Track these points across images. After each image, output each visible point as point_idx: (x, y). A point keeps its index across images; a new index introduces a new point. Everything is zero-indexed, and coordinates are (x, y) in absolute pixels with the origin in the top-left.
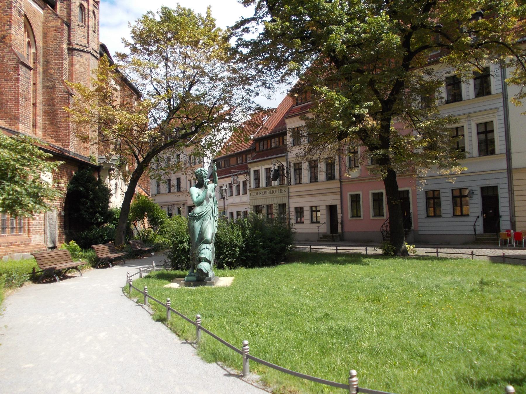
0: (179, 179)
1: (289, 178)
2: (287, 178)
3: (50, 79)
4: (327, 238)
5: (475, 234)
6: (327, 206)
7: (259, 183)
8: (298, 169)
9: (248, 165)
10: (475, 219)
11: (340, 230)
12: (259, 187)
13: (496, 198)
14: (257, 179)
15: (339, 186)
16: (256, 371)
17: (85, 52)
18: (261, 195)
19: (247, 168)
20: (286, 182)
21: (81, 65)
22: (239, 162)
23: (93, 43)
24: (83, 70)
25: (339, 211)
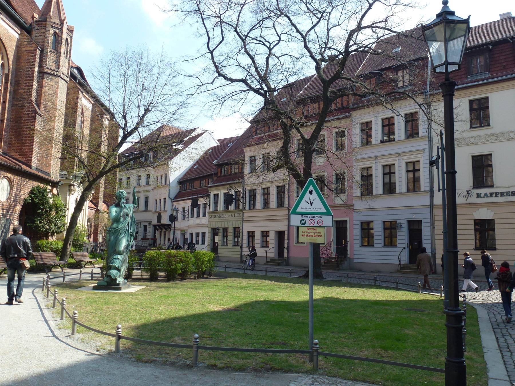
0: (147, 198)
1: (244, 204)
2: (243, 203)
3: (20, 99)
4: (273, 262)
5: (400, 264)
6: (276, 232)
7: (217, 207)
8: (253, 195)
9: (209, 189)
10: (400, 250)
11: (286, 255)
12: (217, 210)
13: (420, 231)
14: (216, 203)
17: (55, 75)
18: (218, 218)
19: (208, 192)
20: (241, 208)
21: (50, 88)
22: (202, 185)
23: (63, 68)
24: (51, 92)
25: (286, 237)
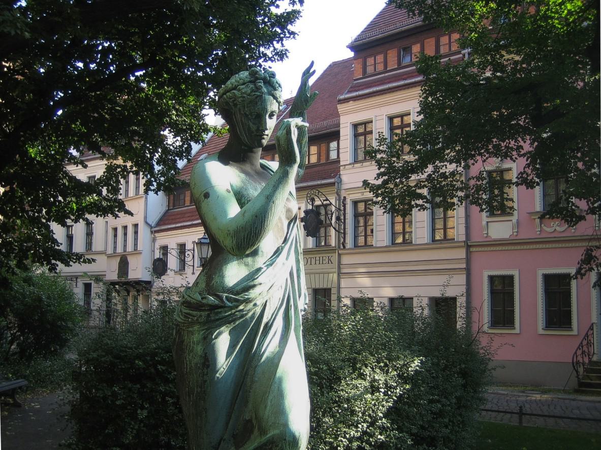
1: (341, 233)
2: (337, 231)
15: (464, 256)
16: (477, 134)
20: (333, 242)
